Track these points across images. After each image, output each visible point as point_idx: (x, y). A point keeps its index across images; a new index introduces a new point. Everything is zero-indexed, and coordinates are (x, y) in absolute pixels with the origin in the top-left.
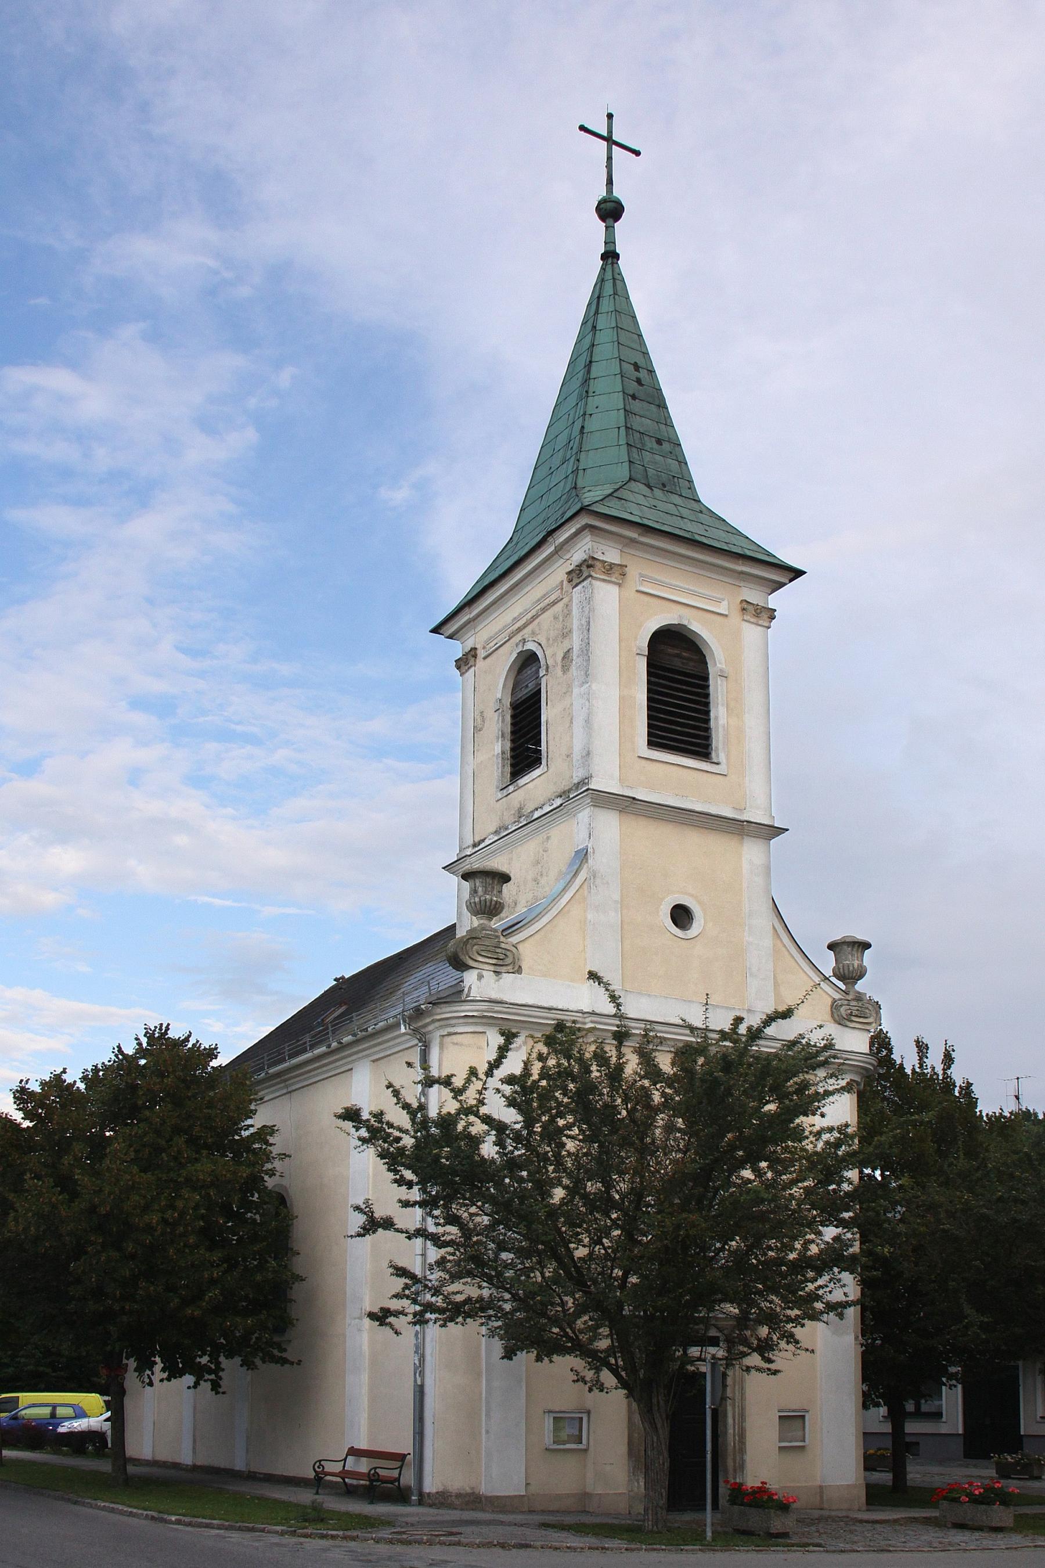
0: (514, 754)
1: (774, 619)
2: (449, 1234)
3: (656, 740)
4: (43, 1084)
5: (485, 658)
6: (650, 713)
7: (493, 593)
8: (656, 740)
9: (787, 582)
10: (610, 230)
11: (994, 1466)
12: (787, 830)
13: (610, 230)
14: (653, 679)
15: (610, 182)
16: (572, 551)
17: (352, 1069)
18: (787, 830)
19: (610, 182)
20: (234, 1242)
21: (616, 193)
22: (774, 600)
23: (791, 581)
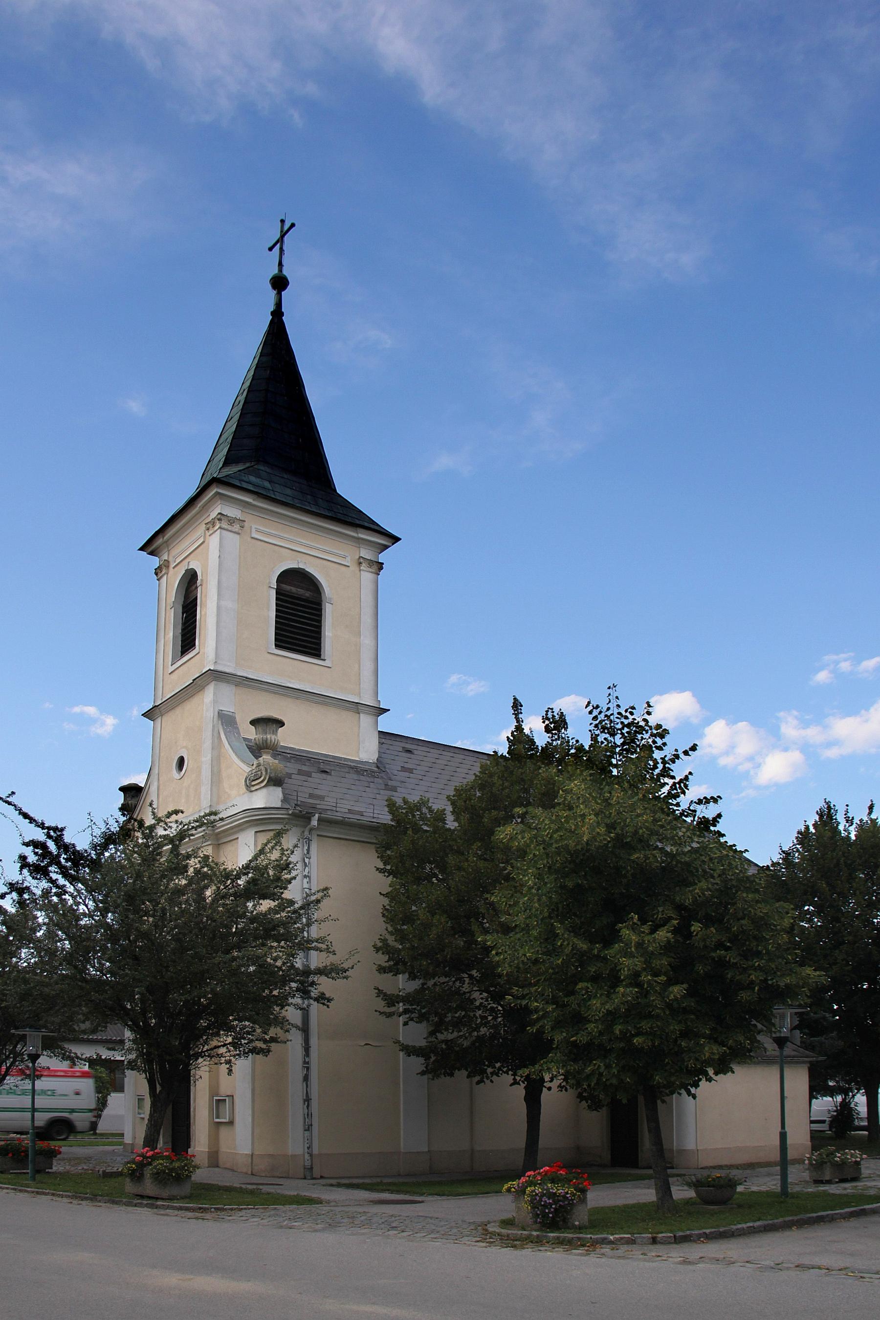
0: (184, 638)
1: (382, 569)
2: (810, 970)
3: (281, 642)
4: (546, 744)
5: (174, 568)
6: (277, 625)
7: (180, 522)
8: (281, 642)
9: (391, 544)
10: (279, 295)
11: (654, 1187)
12: (389, 710)
13: (279, 295)
14: (279, 602)
15: (280, 264)
16: (210, 511)
17: (238, 838)
18: (389, 710)
19: (280, 264)
20: (474, 973)
21: (285, 272)
22: (382, 558)
23: (393, 544)
